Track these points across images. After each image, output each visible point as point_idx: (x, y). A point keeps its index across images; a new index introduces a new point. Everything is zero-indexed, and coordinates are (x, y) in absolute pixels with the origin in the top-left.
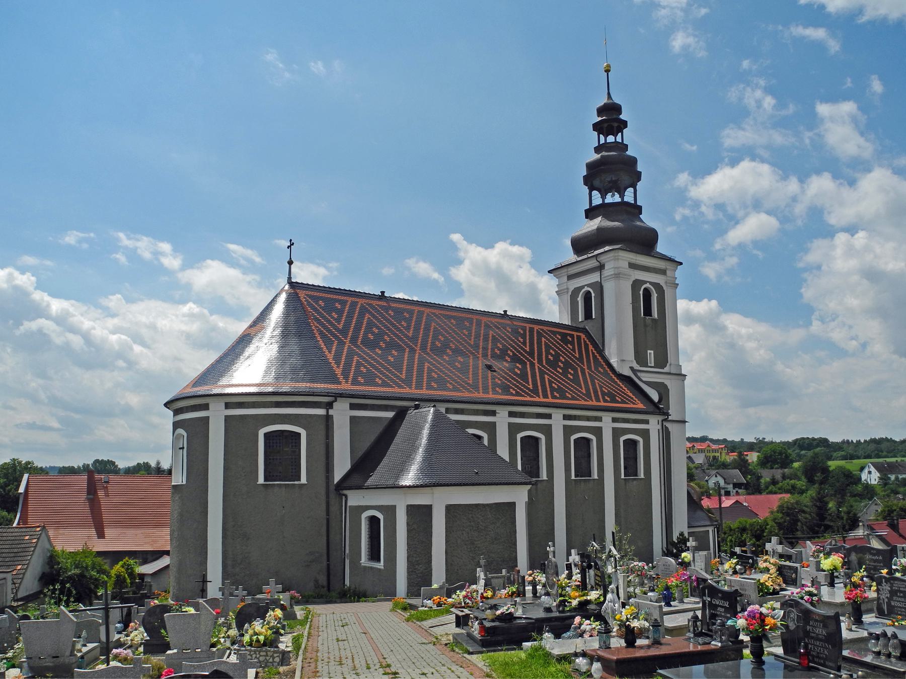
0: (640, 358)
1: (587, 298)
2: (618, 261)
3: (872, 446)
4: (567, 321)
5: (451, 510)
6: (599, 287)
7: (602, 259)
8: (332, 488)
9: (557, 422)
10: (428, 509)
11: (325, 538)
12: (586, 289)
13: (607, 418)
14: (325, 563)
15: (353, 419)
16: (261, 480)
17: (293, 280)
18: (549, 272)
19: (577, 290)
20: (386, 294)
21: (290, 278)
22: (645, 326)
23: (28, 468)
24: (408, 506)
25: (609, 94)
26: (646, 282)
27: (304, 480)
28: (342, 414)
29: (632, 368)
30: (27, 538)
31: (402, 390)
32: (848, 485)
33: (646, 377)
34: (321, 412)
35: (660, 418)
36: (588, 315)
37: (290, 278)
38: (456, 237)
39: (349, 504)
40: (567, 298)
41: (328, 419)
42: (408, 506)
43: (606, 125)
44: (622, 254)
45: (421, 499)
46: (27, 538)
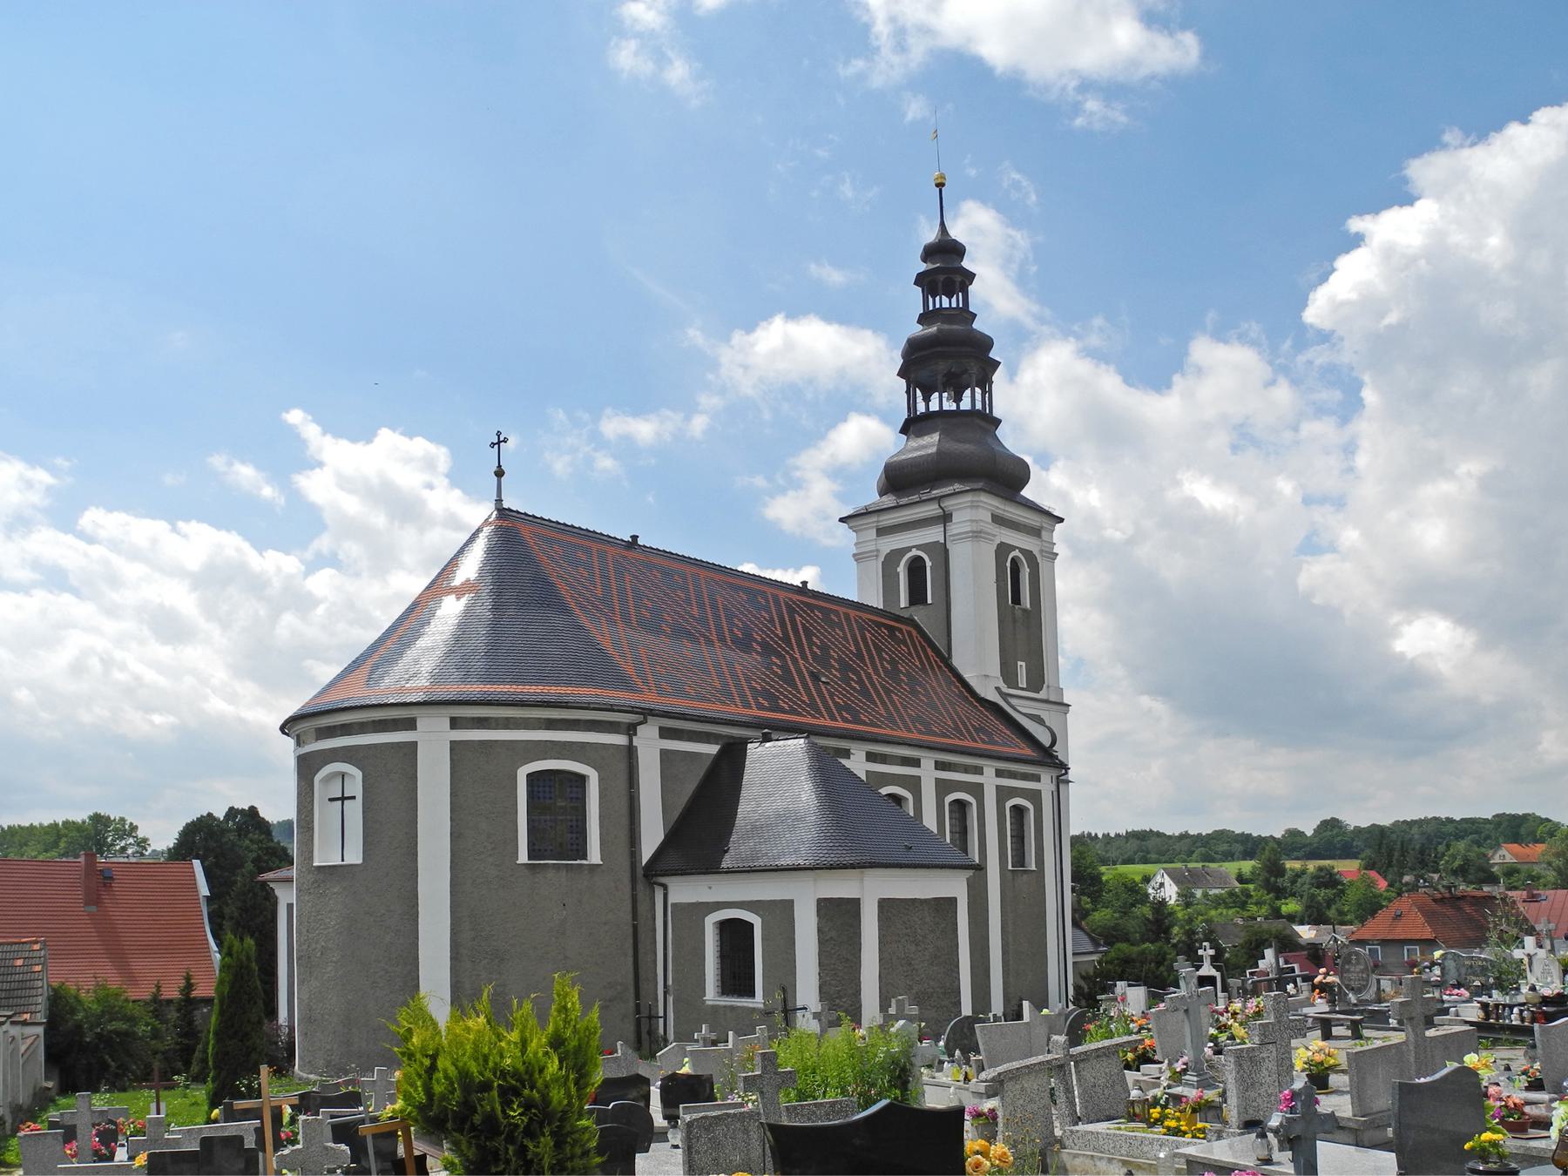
0: (1008, 675)
1: (916, 568)
2: (972, 511)
3: (1133, 845)
4: (876, 601)
5: (885, 905)
6: (941, 552)
7: (949, 504)
8: (640, 872)
9: (928, 773)
10: (853, 906)
11: (630, 960)
12: (914, 552)
13: (989, 768)
14: (631, 1004)
15: (665, 754)
16: (523, 857)
17: (505, 505)
18: (841, 520)
19: (893, 558)
20: (640, 542)
21: (499, 501)
22: (1015, 621)
23: (1061, 780)
24: (819, 901)
25: (942, 224)
26: (1014, 548)
27: (594, 856)
28: (649, 745)
29: (997, 689)
30: (19, 962)
31: (727, 709)
32: (1133, 905)
33: (1021, 709)
34: (620, 740)
35: (1055, 773)
36: (917, 595)
37: (499, 501)
38: (295, 417)
39: (671, 900)
40: (876, 567)
41: (631, 751)
42: (819, 901)
43: (942, 278)
44: (986, 499)
45: (840, 887)
46: (19, 962)
